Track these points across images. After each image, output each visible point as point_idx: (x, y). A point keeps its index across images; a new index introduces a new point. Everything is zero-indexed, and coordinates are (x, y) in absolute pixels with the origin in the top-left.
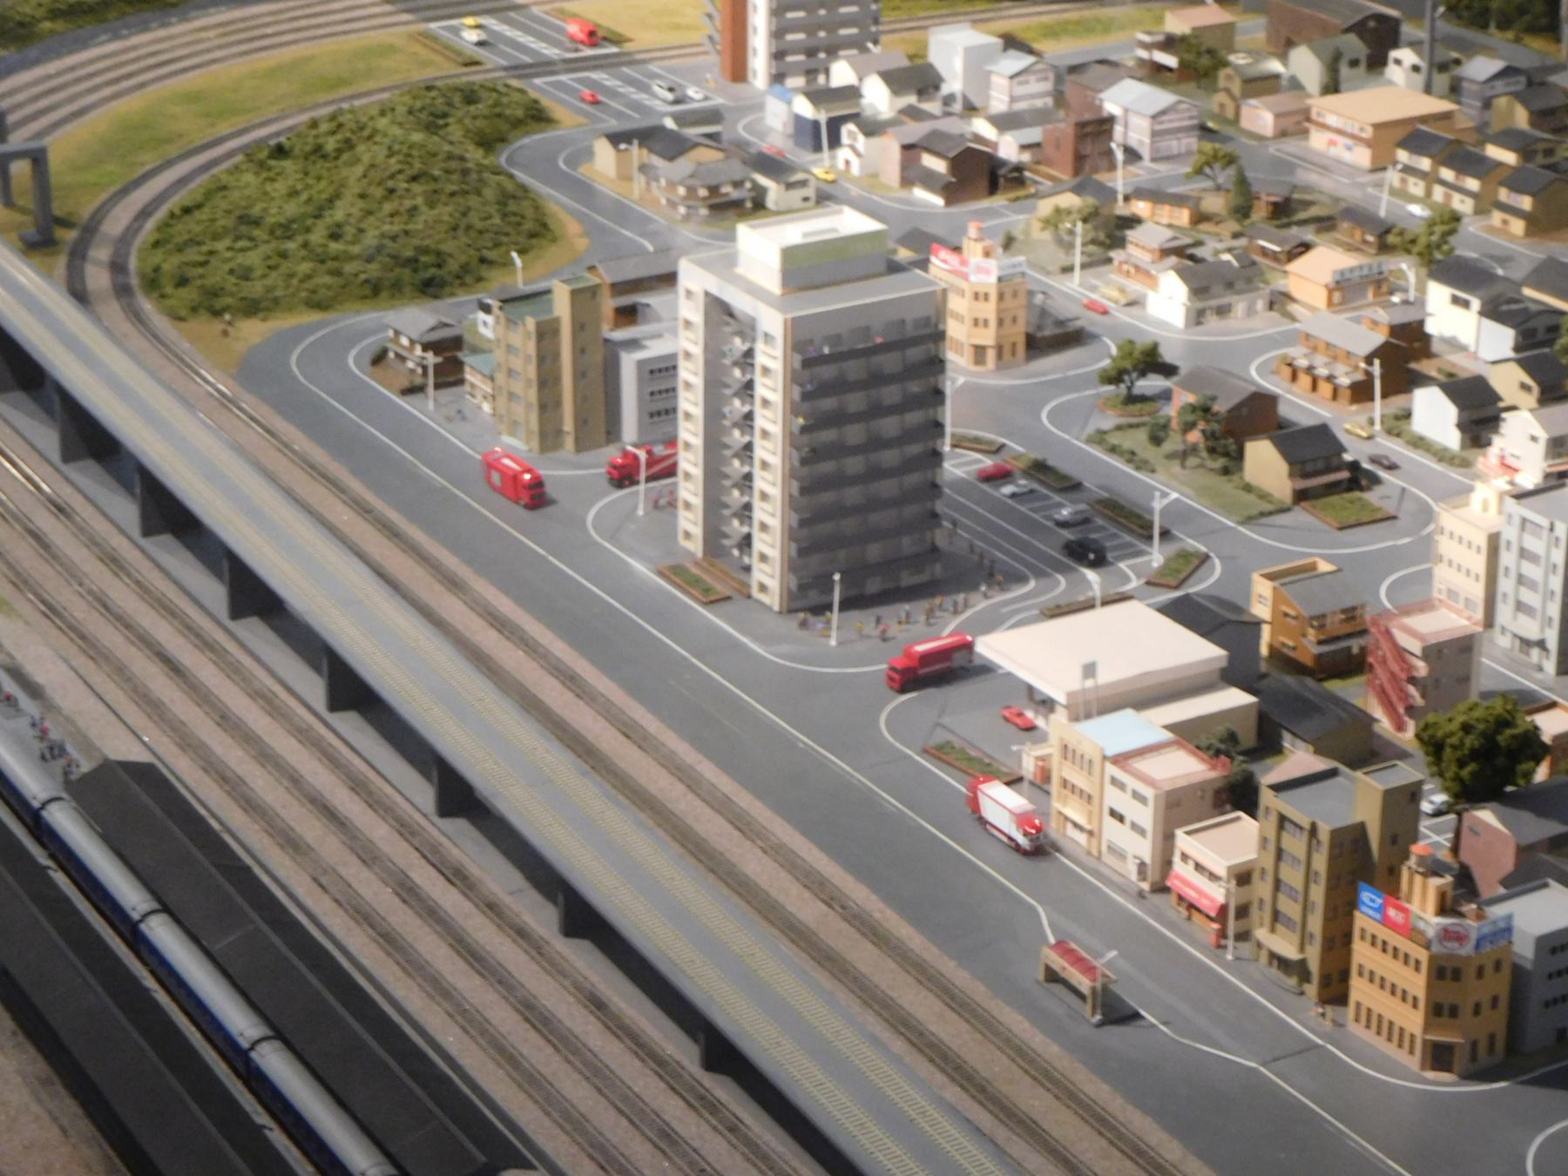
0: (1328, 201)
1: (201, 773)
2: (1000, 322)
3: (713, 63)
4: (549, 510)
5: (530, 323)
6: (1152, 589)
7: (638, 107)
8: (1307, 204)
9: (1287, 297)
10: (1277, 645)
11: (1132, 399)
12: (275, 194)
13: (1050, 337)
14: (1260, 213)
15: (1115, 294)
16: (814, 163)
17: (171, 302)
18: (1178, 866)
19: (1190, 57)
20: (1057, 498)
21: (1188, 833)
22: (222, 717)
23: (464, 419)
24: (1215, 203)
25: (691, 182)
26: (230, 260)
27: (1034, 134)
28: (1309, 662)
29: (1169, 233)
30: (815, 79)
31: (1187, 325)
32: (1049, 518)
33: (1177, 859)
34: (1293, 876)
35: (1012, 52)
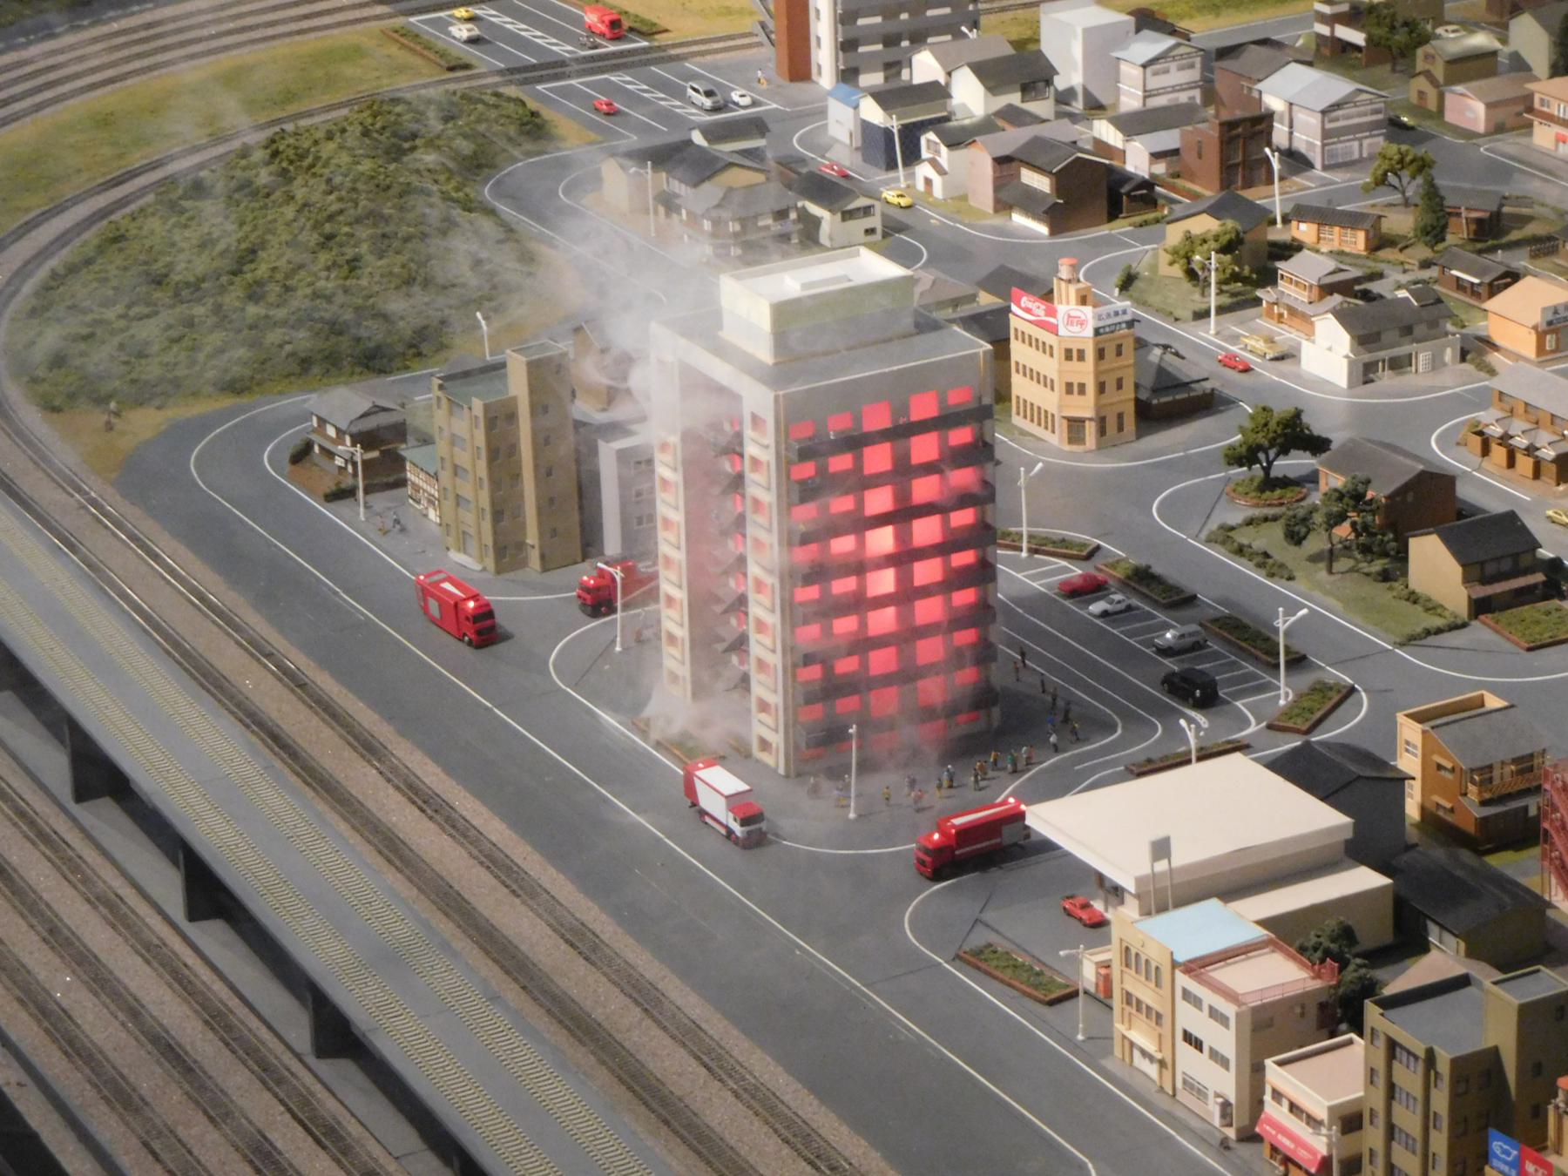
0: (1553, 216)
1: (16, 1005)
2: (1101, 388)
3: (767, 58)
4: (501, 648)
5: (478, 405)
6: (1272, 733)
7: (667, 116)
8: (1525, 220)
9: (1488, 344)
10: (1430, 806)
11: (1270, 483)
12: (185, 245)
13: (1168, 402)
14: (1457, 235)
15: (1260, 345)
16: (886, 183)
17: (45, 387)
18: (1271, 1108)
19: (1380, 32)
20: (1162, 617)
21: (1281, 1064)
22: (51, 931)
23: (403, 530)
24: (1401, 222)
25: (714, 214)
26: (122, 331)
27: (1169, 139)
28: (1470, 828)
29: (1331, 265)
30: (899, 73)
31: (1351, 385)
32: (1150, 643)
33: (1268, 1097)
34: (1408, 1119)
35: (1146, 33)
